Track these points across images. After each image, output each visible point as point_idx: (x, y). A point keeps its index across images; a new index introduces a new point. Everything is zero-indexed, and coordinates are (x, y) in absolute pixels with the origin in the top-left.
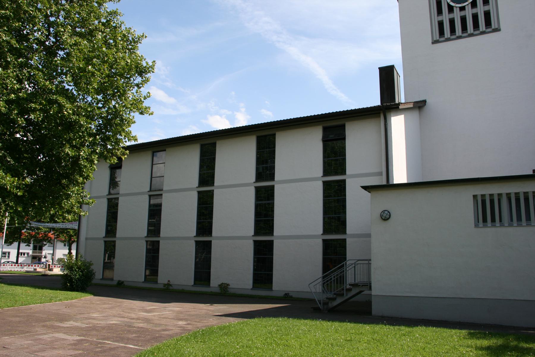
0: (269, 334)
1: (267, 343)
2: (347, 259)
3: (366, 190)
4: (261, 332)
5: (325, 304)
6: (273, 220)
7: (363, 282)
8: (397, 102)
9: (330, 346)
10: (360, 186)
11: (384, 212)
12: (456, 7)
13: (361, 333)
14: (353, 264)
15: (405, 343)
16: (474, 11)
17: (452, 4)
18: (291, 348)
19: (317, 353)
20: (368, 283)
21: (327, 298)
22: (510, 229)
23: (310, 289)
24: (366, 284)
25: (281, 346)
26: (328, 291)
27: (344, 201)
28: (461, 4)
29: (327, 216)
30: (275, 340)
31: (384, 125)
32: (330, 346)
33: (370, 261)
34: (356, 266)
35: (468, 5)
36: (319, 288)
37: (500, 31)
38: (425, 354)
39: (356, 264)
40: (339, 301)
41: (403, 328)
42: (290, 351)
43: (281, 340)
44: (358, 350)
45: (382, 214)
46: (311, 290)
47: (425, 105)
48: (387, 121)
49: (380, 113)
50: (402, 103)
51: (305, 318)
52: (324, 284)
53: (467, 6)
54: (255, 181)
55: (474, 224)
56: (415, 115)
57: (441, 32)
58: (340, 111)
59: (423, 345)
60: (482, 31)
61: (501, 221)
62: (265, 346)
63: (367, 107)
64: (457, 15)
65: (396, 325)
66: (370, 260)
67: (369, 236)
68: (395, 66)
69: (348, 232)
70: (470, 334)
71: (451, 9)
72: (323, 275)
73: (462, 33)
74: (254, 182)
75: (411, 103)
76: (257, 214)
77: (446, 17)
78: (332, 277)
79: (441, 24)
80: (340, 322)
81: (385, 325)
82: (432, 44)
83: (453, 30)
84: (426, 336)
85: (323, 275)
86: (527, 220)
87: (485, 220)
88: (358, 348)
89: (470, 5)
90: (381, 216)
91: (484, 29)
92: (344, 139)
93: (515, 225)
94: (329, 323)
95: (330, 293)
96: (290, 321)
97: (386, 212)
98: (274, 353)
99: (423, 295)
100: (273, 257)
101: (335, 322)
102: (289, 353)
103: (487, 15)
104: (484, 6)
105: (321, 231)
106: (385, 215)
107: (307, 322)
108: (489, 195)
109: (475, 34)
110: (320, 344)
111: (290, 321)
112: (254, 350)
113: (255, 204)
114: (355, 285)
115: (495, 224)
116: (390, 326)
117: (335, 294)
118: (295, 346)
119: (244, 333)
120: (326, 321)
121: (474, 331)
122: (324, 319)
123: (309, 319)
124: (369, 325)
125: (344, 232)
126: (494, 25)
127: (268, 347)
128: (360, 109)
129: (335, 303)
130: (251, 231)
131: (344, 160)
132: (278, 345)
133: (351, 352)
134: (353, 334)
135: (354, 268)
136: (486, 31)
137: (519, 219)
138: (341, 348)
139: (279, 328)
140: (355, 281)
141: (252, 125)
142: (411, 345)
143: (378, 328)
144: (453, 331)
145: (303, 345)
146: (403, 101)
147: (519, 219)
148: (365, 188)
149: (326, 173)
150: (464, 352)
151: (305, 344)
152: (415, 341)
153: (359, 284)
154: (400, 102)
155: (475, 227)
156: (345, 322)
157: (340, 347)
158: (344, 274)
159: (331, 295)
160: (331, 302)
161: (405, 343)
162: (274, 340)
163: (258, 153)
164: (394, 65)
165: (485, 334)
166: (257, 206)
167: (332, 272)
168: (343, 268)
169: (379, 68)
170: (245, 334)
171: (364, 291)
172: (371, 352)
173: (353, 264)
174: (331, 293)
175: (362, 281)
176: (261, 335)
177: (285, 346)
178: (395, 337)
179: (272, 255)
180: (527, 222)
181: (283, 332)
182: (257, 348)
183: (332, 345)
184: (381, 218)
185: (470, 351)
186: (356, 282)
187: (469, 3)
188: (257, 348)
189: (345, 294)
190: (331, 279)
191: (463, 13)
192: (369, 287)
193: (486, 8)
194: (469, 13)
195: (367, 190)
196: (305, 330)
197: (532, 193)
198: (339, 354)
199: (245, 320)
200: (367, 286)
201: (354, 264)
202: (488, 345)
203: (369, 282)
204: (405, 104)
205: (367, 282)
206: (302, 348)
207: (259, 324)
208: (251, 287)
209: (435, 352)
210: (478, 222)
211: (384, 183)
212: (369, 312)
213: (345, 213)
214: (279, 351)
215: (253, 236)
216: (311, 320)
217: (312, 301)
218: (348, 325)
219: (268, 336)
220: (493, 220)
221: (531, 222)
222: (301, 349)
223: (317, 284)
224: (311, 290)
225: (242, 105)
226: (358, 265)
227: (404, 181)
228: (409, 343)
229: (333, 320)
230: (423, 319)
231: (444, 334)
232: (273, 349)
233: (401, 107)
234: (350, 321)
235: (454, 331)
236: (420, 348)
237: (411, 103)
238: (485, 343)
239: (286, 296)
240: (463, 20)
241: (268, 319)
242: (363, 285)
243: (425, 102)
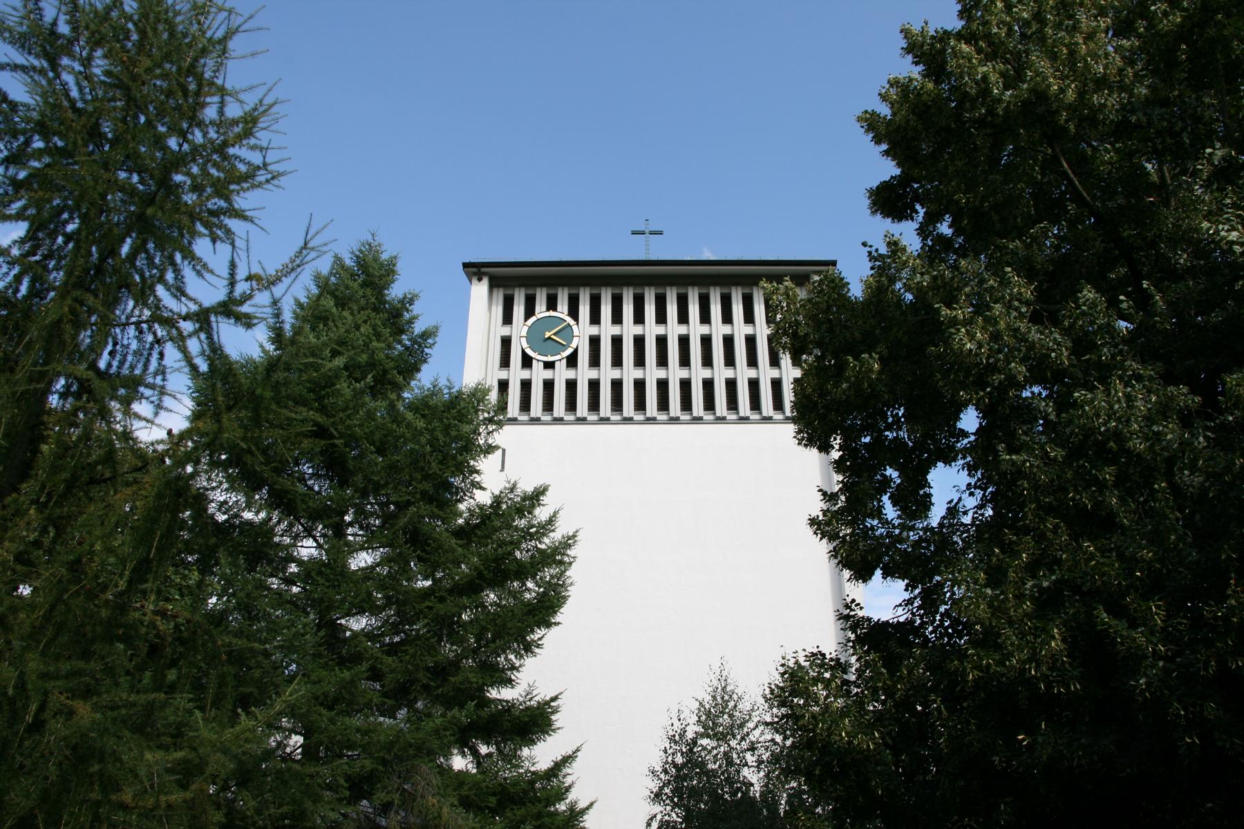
17: (529, 352)
71: (527, 362)
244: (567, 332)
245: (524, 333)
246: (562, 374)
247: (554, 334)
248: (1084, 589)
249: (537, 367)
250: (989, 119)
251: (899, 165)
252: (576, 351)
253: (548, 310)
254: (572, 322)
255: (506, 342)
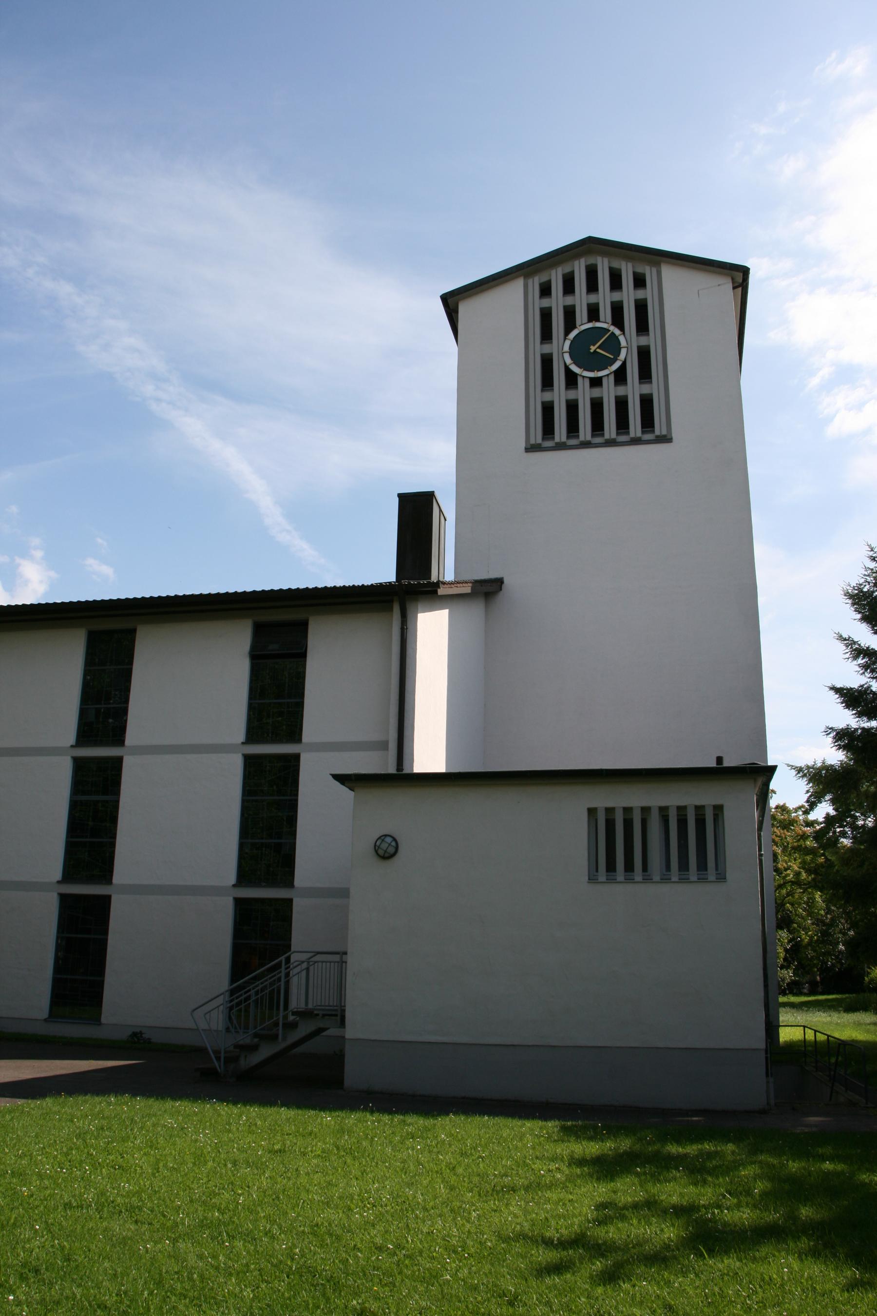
0: (77, 1139)
1: (70, 1162)
2: (293, 949)
3: (343, 783)
4: (57, 1135)
5: (231, 1059)
6: (113, 845)
7: (327, 1008)
8: (434, 578)
9: (229, 1166)
10: (331, 775)
11: (383, 838)
12: (584, 377)
13: (310, 1134)
14: (303, 962)
15: (413, 1154)
16: (621, 391)
17: (575, 369)
18: (130, 1174)
19: (195, 1186)
20: (336, 1010)
21: (236, 1046)
22: (665, 888)
23: (195, 1021)
24: (334, 1013)
25: (104, 1170)
26: (240, 1028)
27: (293, 806)
28: (594, 371)
29: (250, 841)
30: (92, 1155)
31: (400, 630)
32: (229, 1166)
33: (344, 956)
34: (311, 968)
35: (608, 375)
36: (218, 1020)
37: (671, 442)
38: (453, 1180)
39: (311, 963)
40: (266, 1051)
41: (411, 1119)
42: (128, 1181)
43: (106, 1153)
44: (298, 1175)
45: (378, 843)
46: (197, 1026)
47: (501, 590)
48: (408, 620)
49: (392, 601)
50: (444, 583)
51: (176, 1095)
52: (231, 1008)
53: (606, 377)
54: (74, 744)
55: (587, 874)
56: (475, 610)
57: (548, 429)
58: (316, 587)
59: (452, 1160)
60: (583, 441)
61: (645, 868)
62: (62, 1171)
63: (363, 585)
64: (584, 395)
65: (396, 1112)
66: (345, 953)
67: (344, 893)
68: (437, 494)
69: (297, 883)
70: (564, 1129)
71: (571, 380)
72: (231, 985)
73: (593, 436)
74: (72, 746)
75: (466, 583)
76: (75, 826)
77: (559, 395)
78: (252, 992)
79: (548, 410)
80: (264, 1106)
81: (372, 1112)
82: (526, 452)
83: (598, 425)
84: (463, 1138)
85: (231, 985)
86: (699, 869)
87: (611, 867)
88: (297, 1170)
89: (612, 378)
90: (376, 849)
91: (639, 434)
92: (303, 655)
93: (675, 878)
94: (235, 1110)
95: (244, 1032)
96: (137, 1104)
97: (389, 840)
98: (85, 1187)
99: (465, 1039)
100: (107, 940)
101: (251, 1106)
102: (124, 1185)
103: (647, 402)
104: (640, 383)
105: (232, 878)
106: (384, 846)
107: (180, 1105)
108: (622, 809)
109: (545, 446)
110: (206, 1162)
111: (137, 1104)
112: (30, 1183)
113: (71, 801)
114: (306, 1014)
115: (633, 875)
116: (383, 1115)
117: (256, 1035)
118: (142, 1167)
119: (12, 1139)
120: (228, 1104)
121: (574, 1123)
122: (223, 1098)
123: (187, 1098)
124: (334, 1114)
125: (288, 879)
126: (659, 428)
127: (71, 1173)
128: (347, 587)
129: (256, 1058)
130: (54, 869)
131: (300, 705)
132: (96, 1166)
133: (279, 1179)
134: (290, 1134)
135: (305, 971)
136: (643, 439)
137: (684, 866)
138: (256, 1172)
139: (105, 1123)
140: (307, 1003)
141: (176, 596)
142: (426, 1160)
143: (351, 1119)
144: (526, 1123)
145: (161, 1165)
146: (449, 575)
147: (684, 866)
148: (342, 779)
149: (254, 734)
150: (542, 1172)
151: (166, 1163)
152: (435, 1150)
153: (316, 1012)
154: (441, 579)
155: (588, 882)
156: (274, 1106)
157: (254, 1168)
158: (280, 985)
159: (245, 1038)
160: (246, 1056)
161: (413, 1154)
162: (89, 1154)
163: (86, 673)
164: (434, 492)
165: (595, 1128)
166: (74, 806)
167: (255, 978)
168: (279, 971)
169: (400, 496)
170: (15, 1141)
171: (329, 1028)
172: (328, 1179)
173: (303, 962)
174: (247, 1033)
175: (331, 1004)
176: (55, 1141)
177: (115, 1169)
178: (391, 1142)
179: (106, 932)
180: (680, 873)
181: (115, 1132)
182: (41, 1176)
183: (235, 1163)
184: (376, 852)
185: (557, 1168)
186: (310, 1006)
187: (611, 373)
188: (41, 1176)
189: (280, 1037)
190: (248, 998)
191: (596, 392)
192: (339, 1018)
193: (646, 389)
194: (609, 393)
195: (346, 785)
196: (173, 1128)
197: (712, 808)
198: (248, 1187)
199: (20, 1102)
200: (336, 1015)
201: (306, 963)
202: (599, 1152)
203: (341, 1006)
204: (452, 586)
205: (335, 1008)
206: (158, 1172)
207: (55, 1113)
208: (45, 1014)
209: (479, 1175)
210: (597, 871)
211: (392, 769)
212: (338, 1082)
213: (293, 834)
214: (97, 1181)
215: (58, 882)
216: (190, 1100)
217: (201, 1051)
218: (282, 1114)
219: (75, 1144)
220: (629, 867)
221: (707, 874)
222: (157, 1174)
223: (212, 1010)
224: (197, 1026)
225: (36, 541)
226: (316, 964)
227: (438, 765)
228: (420, 1156)
229: (247, 1100)
230: (464, 1098)
231: (505, 1133)
232: (82, 1178)
233: (441, 591)
234: (287, 1104)
235: (529, 1124)
236: (444, 1168)
237: (466, 583)
238: (593, 1148)
239: (136, 1039)
240: (597, 406)
241: (81, 1099)
242: (324, 1015)
243: (499, 584)
244: (613, 345)
245: (567, 347)
246: (609, 393)
247: (599, 347)
248: (315, 1284)
249: (583, 385)
250: (845, 823)
251: (835, 809)
252: (624, 364)
253: (590, 320)
254: (617, 332)
255: (547, 362)
